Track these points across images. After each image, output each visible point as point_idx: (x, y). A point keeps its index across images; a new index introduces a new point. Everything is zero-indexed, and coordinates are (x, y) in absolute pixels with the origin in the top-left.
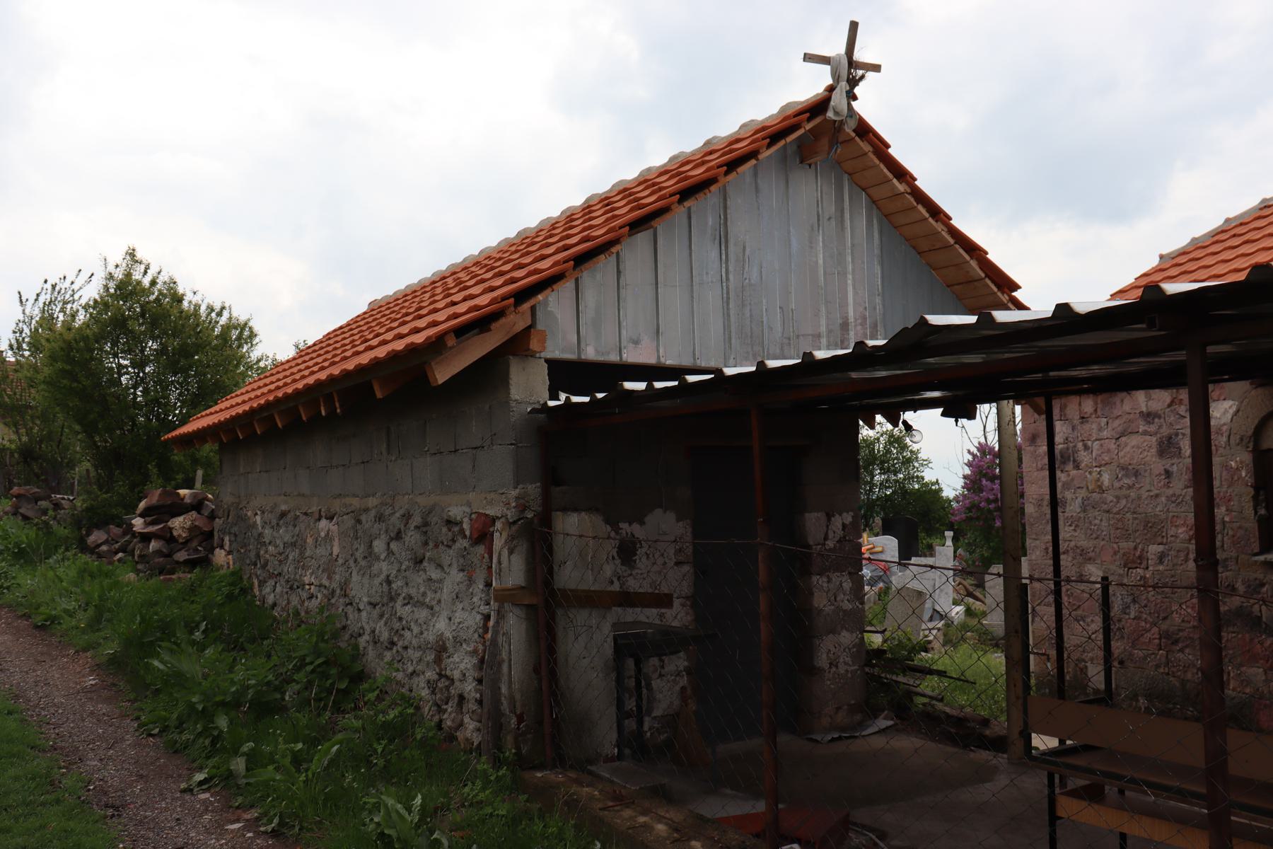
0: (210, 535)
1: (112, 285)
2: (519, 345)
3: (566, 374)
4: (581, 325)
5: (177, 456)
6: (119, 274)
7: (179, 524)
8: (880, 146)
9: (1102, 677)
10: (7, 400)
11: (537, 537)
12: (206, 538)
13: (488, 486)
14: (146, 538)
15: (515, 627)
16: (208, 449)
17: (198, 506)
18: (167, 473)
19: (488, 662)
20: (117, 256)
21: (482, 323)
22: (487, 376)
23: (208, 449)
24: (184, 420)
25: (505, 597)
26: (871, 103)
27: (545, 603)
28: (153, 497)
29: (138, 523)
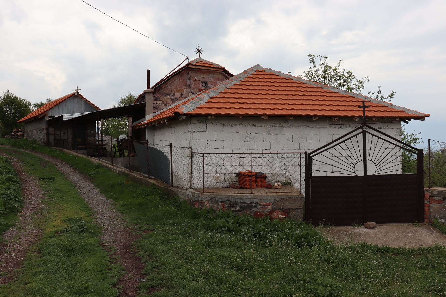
0: (23, 135)
1: (5, 97)
2: (45, 115)
3: (50, 117)
4: (50, 114)
5: (18, 125)
6: (6, 95)
7: (19, 133)
8: (82, 96)
9: (187, 169)
10: (88, 131)
11: (47, 129)
12: (23, 135)
13: (43, 126)
14: (14, 135)
15: (45, 136)
16: (23, 124)
17: (21, 131)
18: (16, 127)
19: (44, 139)
20: (6, 91)
21: (42, 114)
22: (43, 117)
23: (23, 124)
24: (19, 120)
25: (45, 134)
26: (80, 92)
27: (48, 134)
28: (15, 130)
29: (13, 133)
